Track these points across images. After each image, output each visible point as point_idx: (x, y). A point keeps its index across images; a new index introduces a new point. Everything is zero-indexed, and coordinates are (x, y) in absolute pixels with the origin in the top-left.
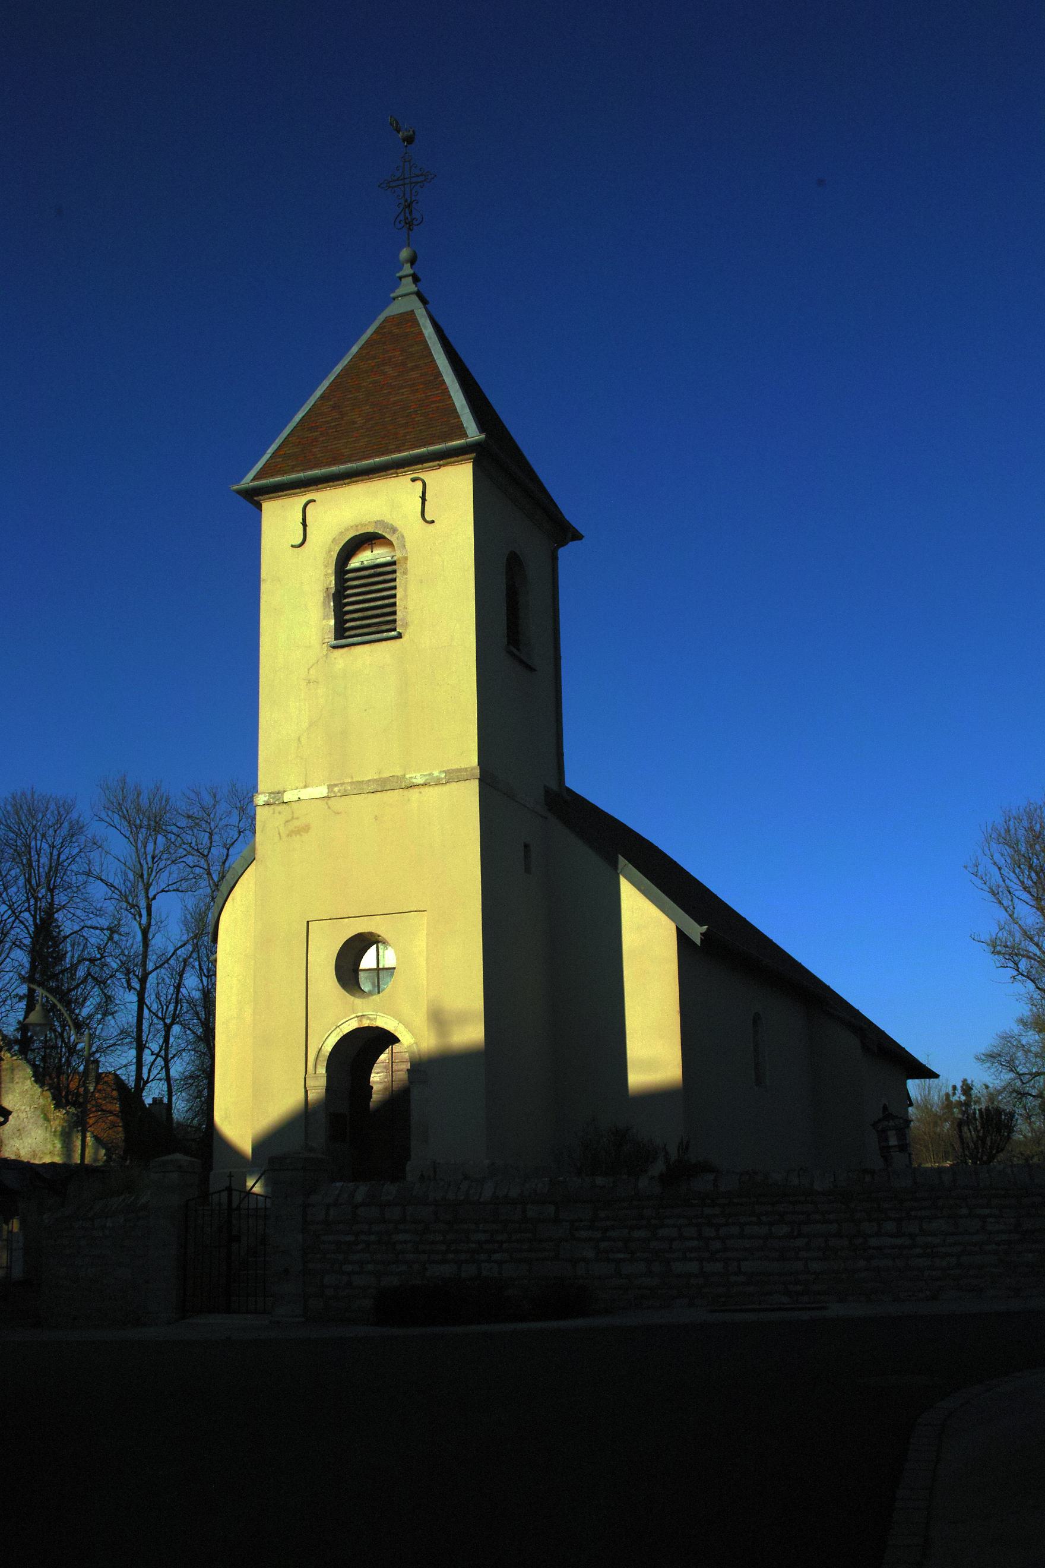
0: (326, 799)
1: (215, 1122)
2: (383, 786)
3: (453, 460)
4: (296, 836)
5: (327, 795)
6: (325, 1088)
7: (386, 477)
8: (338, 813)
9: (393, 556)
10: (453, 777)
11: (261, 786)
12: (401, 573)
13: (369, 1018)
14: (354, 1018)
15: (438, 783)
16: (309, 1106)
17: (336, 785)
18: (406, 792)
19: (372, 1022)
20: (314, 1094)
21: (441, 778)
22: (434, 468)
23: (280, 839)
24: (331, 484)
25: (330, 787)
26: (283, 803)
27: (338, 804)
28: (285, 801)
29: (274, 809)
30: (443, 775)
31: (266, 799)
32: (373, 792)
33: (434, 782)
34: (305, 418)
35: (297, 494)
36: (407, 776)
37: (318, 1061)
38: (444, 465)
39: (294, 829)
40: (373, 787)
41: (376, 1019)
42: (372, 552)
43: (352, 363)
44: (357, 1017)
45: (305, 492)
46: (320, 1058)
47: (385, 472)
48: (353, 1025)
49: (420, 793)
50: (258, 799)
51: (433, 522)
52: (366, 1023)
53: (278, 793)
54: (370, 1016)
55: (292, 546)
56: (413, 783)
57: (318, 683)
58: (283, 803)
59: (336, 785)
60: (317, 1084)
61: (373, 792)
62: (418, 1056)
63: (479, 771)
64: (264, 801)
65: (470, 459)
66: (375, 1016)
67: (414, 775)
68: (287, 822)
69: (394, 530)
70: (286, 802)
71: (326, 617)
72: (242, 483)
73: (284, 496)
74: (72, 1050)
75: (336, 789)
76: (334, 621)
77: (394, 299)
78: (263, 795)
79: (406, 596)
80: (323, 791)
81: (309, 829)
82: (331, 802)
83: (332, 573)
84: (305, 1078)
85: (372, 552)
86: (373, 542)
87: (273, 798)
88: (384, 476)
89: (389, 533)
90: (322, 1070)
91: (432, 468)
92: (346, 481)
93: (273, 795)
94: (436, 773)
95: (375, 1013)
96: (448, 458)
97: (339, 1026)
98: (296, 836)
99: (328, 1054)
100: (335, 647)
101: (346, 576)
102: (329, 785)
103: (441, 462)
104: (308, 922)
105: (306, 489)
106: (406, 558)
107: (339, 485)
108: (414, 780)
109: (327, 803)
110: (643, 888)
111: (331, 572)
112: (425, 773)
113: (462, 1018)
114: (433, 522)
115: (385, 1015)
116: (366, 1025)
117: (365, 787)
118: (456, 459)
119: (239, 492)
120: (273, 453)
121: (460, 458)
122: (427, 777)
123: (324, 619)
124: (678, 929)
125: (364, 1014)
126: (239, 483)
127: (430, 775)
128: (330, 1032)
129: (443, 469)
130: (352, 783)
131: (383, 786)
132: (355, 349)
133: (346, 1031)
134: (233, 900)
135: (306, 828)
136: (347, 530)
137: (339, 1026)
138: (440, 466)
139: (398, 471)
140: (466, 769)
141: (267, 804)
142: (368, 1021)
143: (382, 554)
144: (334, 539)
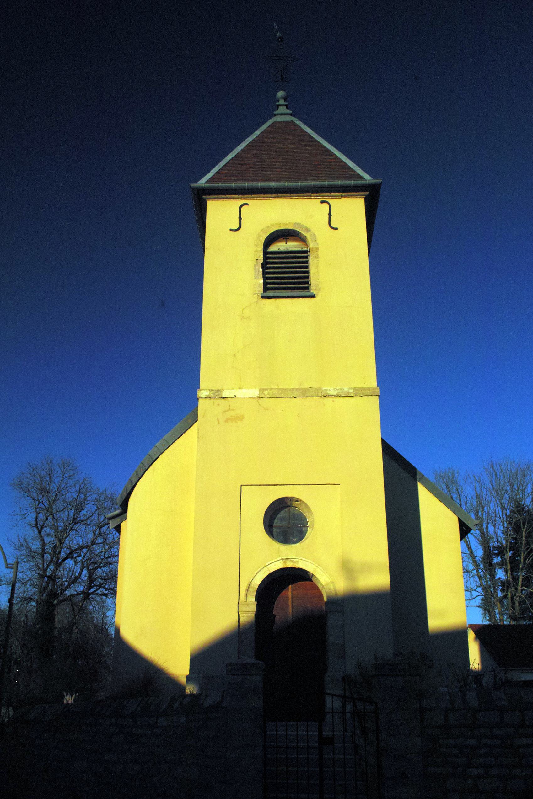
0: (257, 399)
1: (120, 633)
2: (304, 394)
3: (352, 194)
4: (232, 422)
5: (258, 395)
6: (255, 613)
7: (302, 197)
8: (267, 409)
9: (303, 248)
10: (360, 393)
11: (202, 385)
12: (313, 257)
13: (293, 562)
14: (280, 560)
15: (347, 396)
16: (240, 627)
17: (266, 389)
18: (321, 400)
19: (295, 564)
20: (245, 618)
21: (350, 392)
22: (338, 197)
23: (219, 423)
24: (262, 195)
25: (262, 390)
26: (222, 398)
27: (266, 402)
28: (223, 397)
29: (214, 402)
30: (351, 391)
31: (208, 394)
32: (295, 397)
33: (345, 394)
34: (233, 159)
35: (236, 198)
36: (324, 389)
37: (249, 592)
38: (345, 197)
39: (230, 417)
40: (295, 394)
41: (297, 562)
42: (286, 243)
43: (258, 138)
44: (282, 559)
45: (241, 198)
46: (250, 590)
47: (304, 193)
48: (279, 565)
49: (333, 401)
50: (201, 393)
51: (337, 229)
52: (289, 565)
53: (218, 391)
54: (292, 559)
55: (231, 230)
56: (328, 394)
57: (250, 319)
58: (222, 398)
59: (266, 389)
60: (248, 609)
61: (295, 397)
62: (334, 592)
63: (379, 391)
64: (206, 395)
65: (364, 196)
66: (298, 560)
67: (329, 389)
68: (224, 412)
69: (308, 230)
70: (224, 398)
71: (256, 277)
72: (198, 183)
73: (225, 199)
74: (338, 555)
75: (266, 392)
76: (262, 280)
77: (275, 115)
78: (205, 391)
79: (318, 272)
80: (256, 393)
81: (243, 418)
82: (261, 401)
83: (261, 250)
84: (238, 604)
85: (286, 243)
86: (287, 238)
87: (213, 394)
88: (302, 196)
89: (304, 232)
90: (252, 599)
91: (335, 197)
92: (273, 195)
93: (213, 392)
94: (346, 389)
95: (298, 558)
96: (349, 192)
97: (266, 566)
98: (232, 422)
99: (257, 587)
100: (263, 297)
101: (268, 256)
102: (260, 389)
103: (344, 194)
104: (241, 485)
105: (242, 196)
106: (317, 249)
107: (268, 198)
108: (328, 392)
109: (258, 401)
110: (435, 492)
111: (260, 250)
112: (338, 388)
113: (367, 568)
114: (337, 229)
115: (306, 560)
116: (289, 566)
117: (290, 392)
118: (354, 193)
119: (193, 189)
120: (217, 172)
121: (357, 193)
122: (339, 391)
123: (255, 278)
124: (460, 521)
125: (289, 557)
126: (197, 182)
127: (341, 389)
128: (259, 570)
129: (343, 199)
130: (279, 389)
131: (304, 394)
132: (257, 133)
133: (272, 570)
134: (154, 470)
135: (241, 418)
136: (272, 225)
137: (266, 566)
138: (342, 196)
139: (313, 195)
140: (369, 389)
141: (208, 398)
142: (292, 563)
143: (294, 245)
144: (263, 229)
